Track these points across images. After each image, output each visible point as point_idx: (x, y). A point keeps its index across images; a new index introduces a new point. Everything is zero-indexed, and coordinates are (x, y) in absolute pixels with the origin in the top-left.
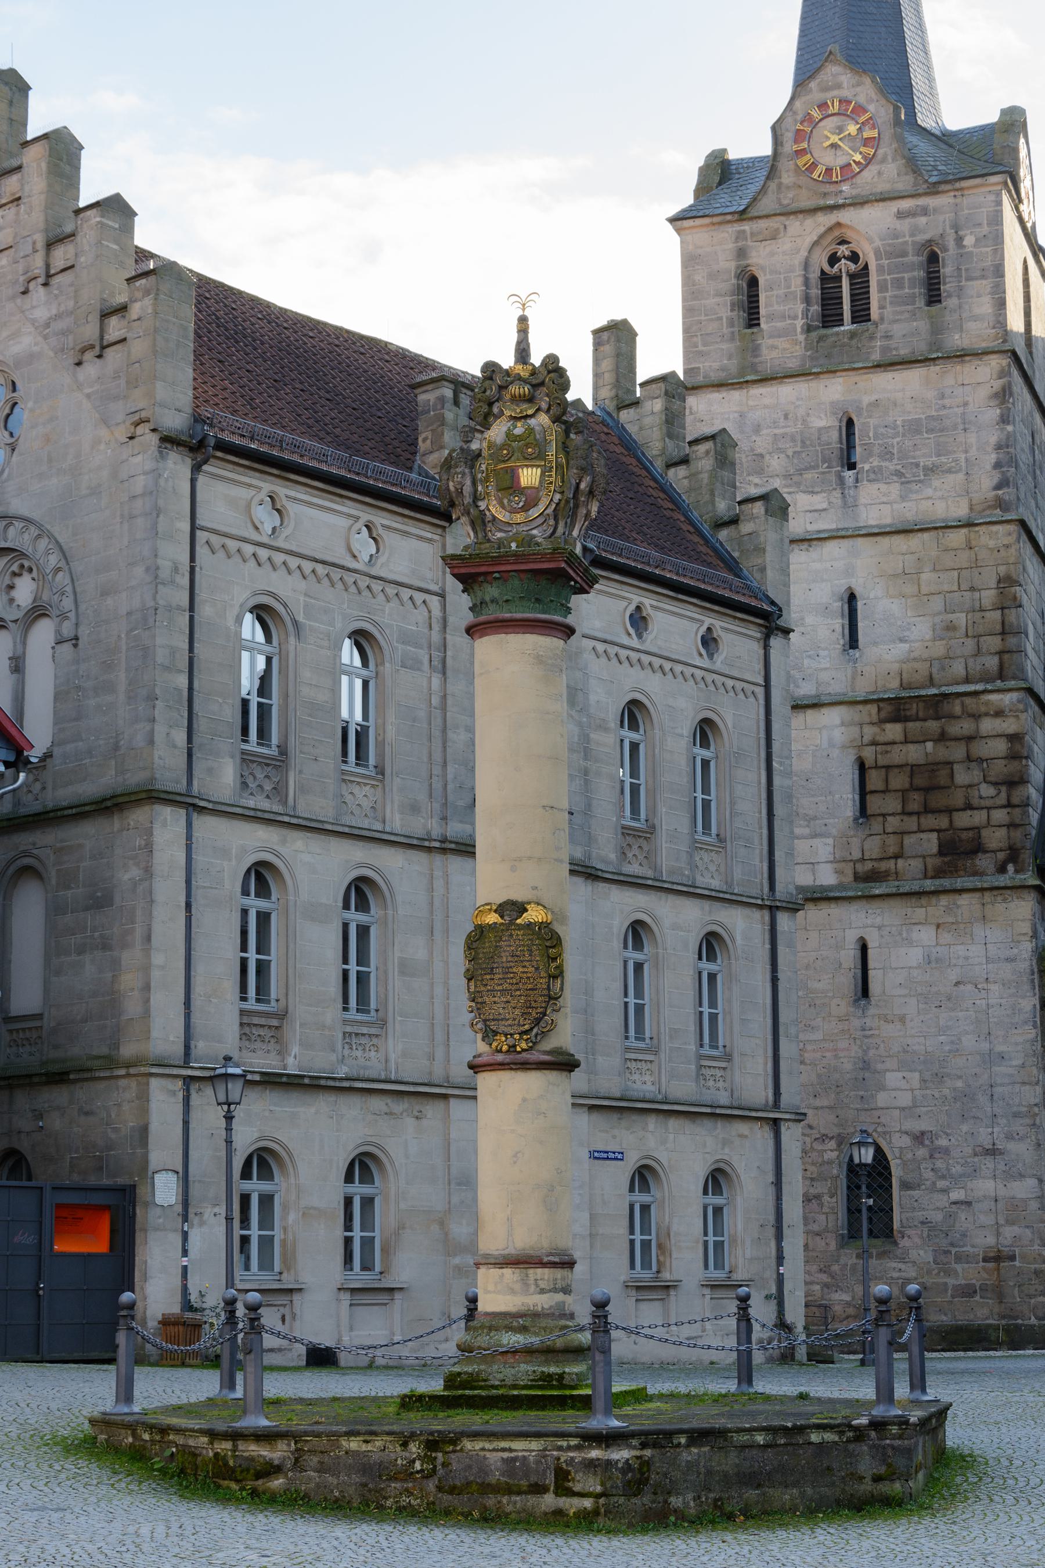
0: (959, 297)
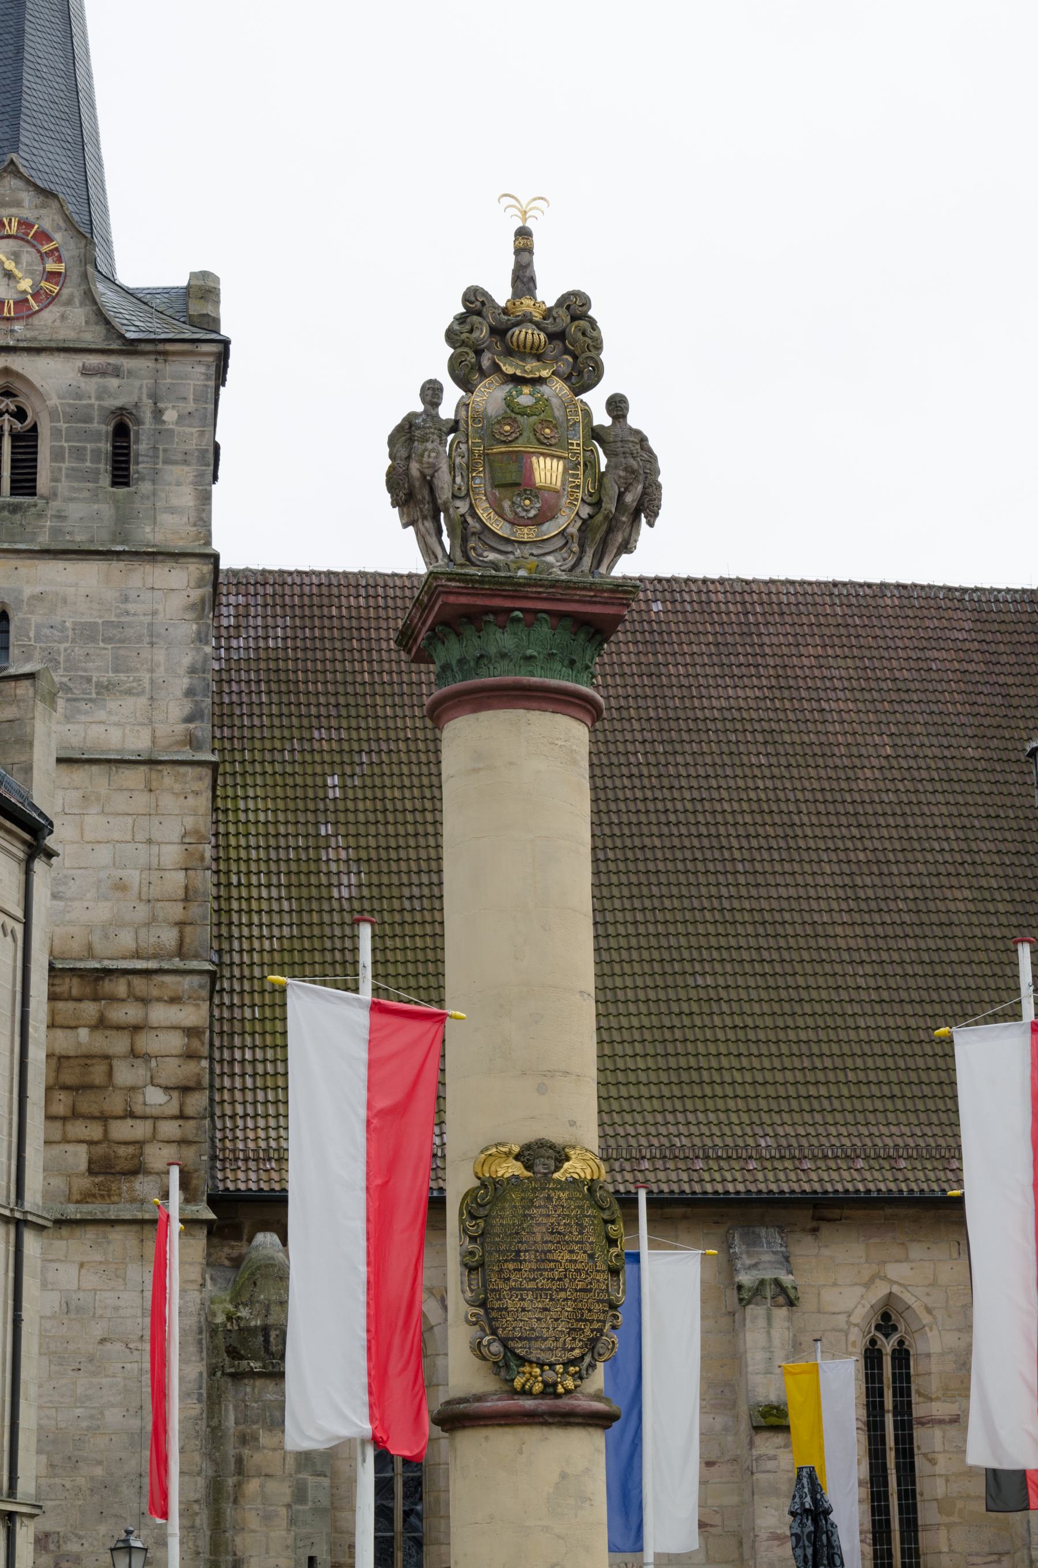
0: (154, 482)
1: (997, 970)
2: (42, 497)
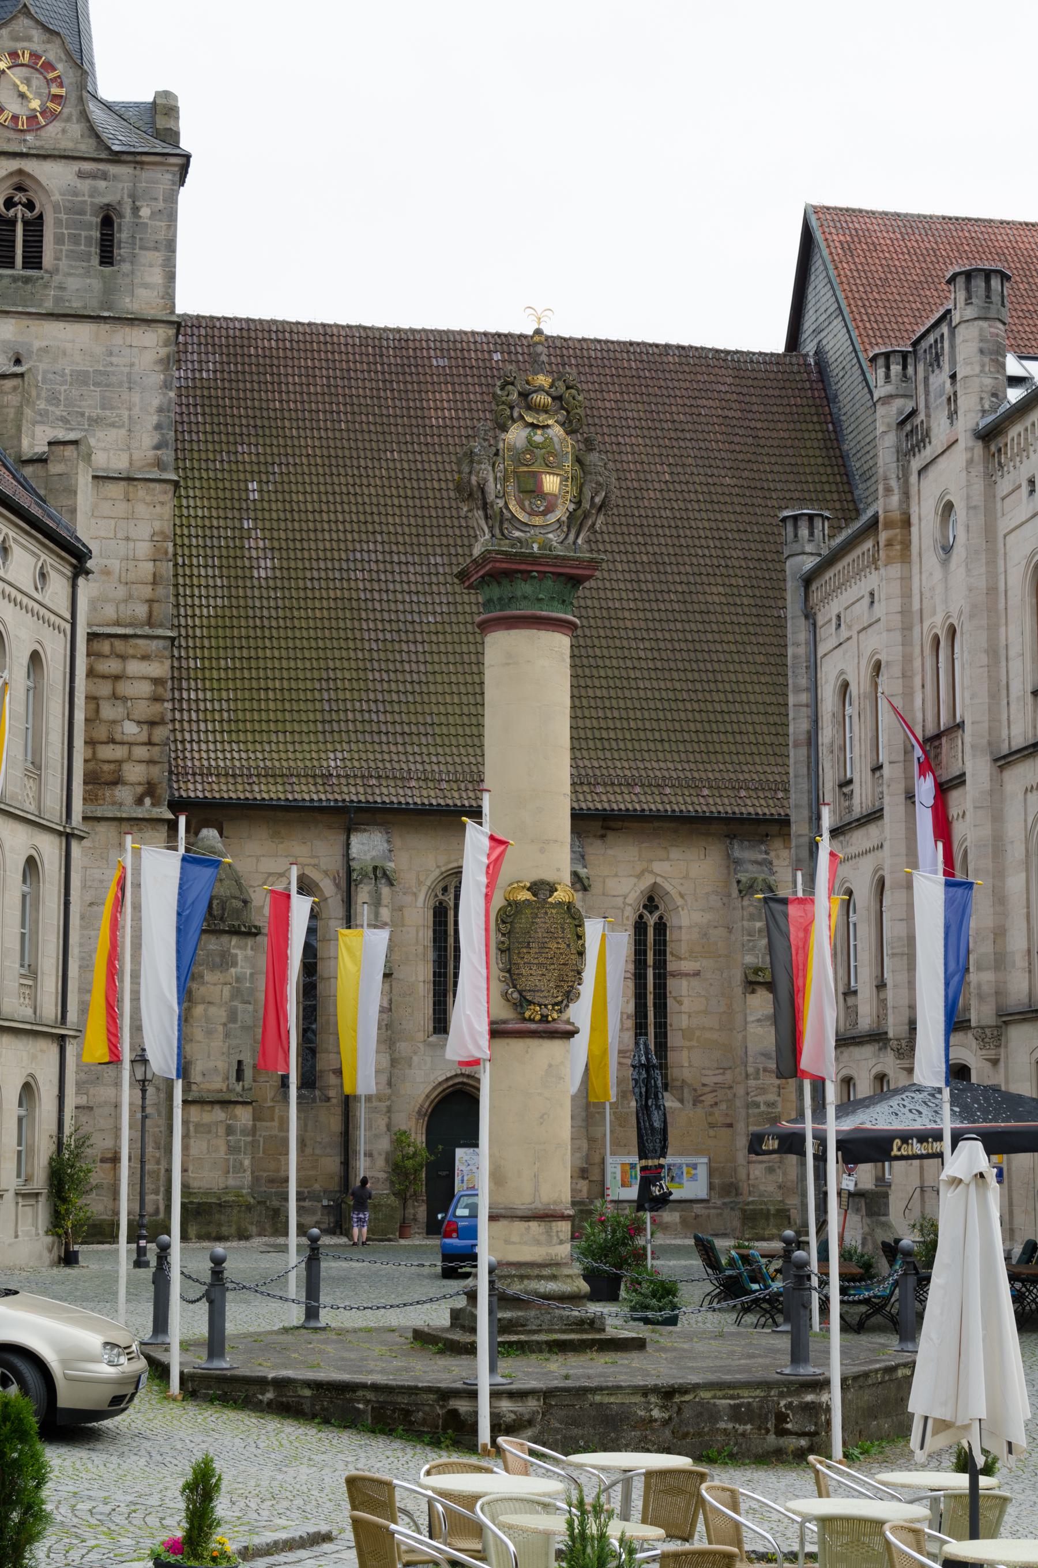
0: (132, 263)
1: (741, 648)
2: (47, 271)
